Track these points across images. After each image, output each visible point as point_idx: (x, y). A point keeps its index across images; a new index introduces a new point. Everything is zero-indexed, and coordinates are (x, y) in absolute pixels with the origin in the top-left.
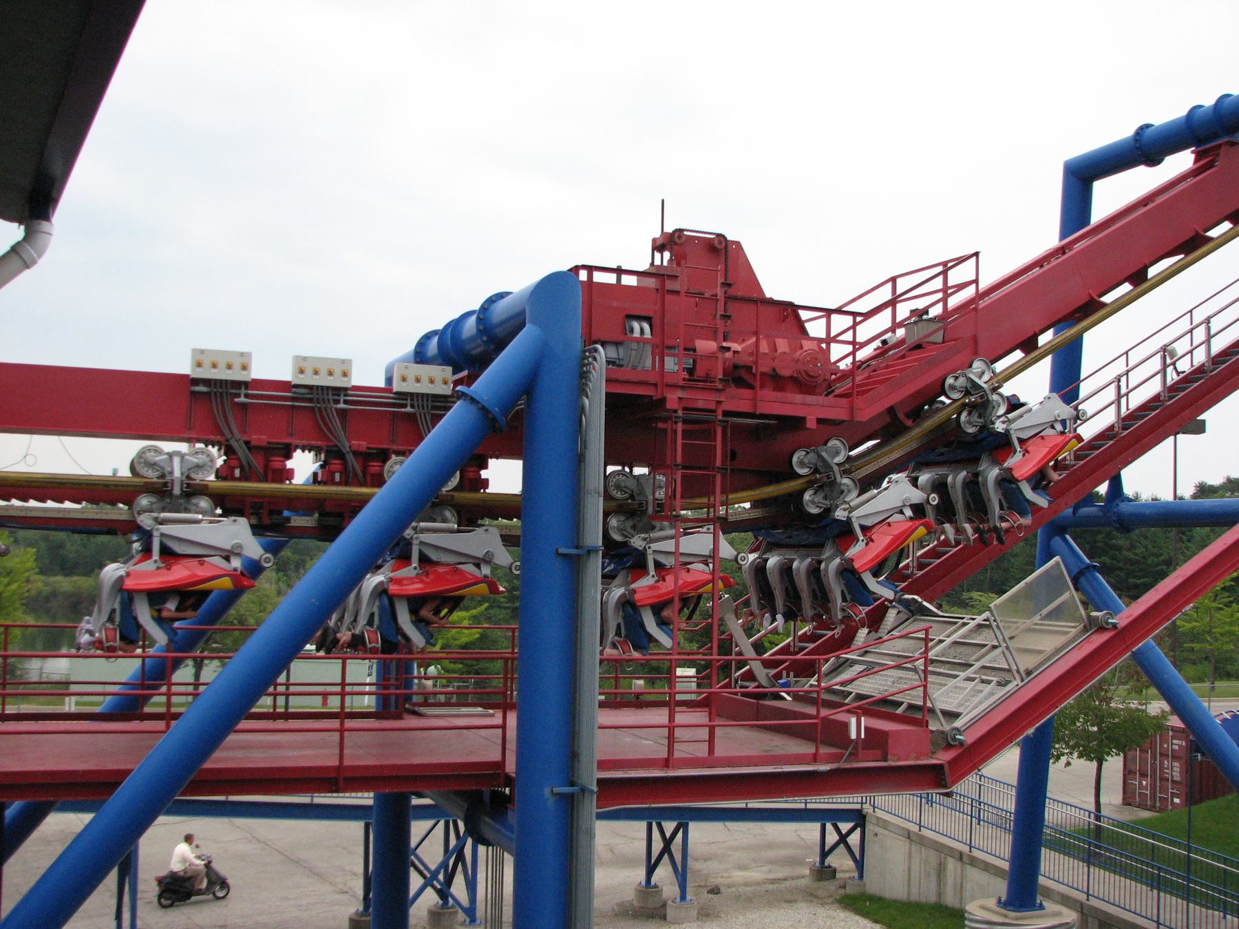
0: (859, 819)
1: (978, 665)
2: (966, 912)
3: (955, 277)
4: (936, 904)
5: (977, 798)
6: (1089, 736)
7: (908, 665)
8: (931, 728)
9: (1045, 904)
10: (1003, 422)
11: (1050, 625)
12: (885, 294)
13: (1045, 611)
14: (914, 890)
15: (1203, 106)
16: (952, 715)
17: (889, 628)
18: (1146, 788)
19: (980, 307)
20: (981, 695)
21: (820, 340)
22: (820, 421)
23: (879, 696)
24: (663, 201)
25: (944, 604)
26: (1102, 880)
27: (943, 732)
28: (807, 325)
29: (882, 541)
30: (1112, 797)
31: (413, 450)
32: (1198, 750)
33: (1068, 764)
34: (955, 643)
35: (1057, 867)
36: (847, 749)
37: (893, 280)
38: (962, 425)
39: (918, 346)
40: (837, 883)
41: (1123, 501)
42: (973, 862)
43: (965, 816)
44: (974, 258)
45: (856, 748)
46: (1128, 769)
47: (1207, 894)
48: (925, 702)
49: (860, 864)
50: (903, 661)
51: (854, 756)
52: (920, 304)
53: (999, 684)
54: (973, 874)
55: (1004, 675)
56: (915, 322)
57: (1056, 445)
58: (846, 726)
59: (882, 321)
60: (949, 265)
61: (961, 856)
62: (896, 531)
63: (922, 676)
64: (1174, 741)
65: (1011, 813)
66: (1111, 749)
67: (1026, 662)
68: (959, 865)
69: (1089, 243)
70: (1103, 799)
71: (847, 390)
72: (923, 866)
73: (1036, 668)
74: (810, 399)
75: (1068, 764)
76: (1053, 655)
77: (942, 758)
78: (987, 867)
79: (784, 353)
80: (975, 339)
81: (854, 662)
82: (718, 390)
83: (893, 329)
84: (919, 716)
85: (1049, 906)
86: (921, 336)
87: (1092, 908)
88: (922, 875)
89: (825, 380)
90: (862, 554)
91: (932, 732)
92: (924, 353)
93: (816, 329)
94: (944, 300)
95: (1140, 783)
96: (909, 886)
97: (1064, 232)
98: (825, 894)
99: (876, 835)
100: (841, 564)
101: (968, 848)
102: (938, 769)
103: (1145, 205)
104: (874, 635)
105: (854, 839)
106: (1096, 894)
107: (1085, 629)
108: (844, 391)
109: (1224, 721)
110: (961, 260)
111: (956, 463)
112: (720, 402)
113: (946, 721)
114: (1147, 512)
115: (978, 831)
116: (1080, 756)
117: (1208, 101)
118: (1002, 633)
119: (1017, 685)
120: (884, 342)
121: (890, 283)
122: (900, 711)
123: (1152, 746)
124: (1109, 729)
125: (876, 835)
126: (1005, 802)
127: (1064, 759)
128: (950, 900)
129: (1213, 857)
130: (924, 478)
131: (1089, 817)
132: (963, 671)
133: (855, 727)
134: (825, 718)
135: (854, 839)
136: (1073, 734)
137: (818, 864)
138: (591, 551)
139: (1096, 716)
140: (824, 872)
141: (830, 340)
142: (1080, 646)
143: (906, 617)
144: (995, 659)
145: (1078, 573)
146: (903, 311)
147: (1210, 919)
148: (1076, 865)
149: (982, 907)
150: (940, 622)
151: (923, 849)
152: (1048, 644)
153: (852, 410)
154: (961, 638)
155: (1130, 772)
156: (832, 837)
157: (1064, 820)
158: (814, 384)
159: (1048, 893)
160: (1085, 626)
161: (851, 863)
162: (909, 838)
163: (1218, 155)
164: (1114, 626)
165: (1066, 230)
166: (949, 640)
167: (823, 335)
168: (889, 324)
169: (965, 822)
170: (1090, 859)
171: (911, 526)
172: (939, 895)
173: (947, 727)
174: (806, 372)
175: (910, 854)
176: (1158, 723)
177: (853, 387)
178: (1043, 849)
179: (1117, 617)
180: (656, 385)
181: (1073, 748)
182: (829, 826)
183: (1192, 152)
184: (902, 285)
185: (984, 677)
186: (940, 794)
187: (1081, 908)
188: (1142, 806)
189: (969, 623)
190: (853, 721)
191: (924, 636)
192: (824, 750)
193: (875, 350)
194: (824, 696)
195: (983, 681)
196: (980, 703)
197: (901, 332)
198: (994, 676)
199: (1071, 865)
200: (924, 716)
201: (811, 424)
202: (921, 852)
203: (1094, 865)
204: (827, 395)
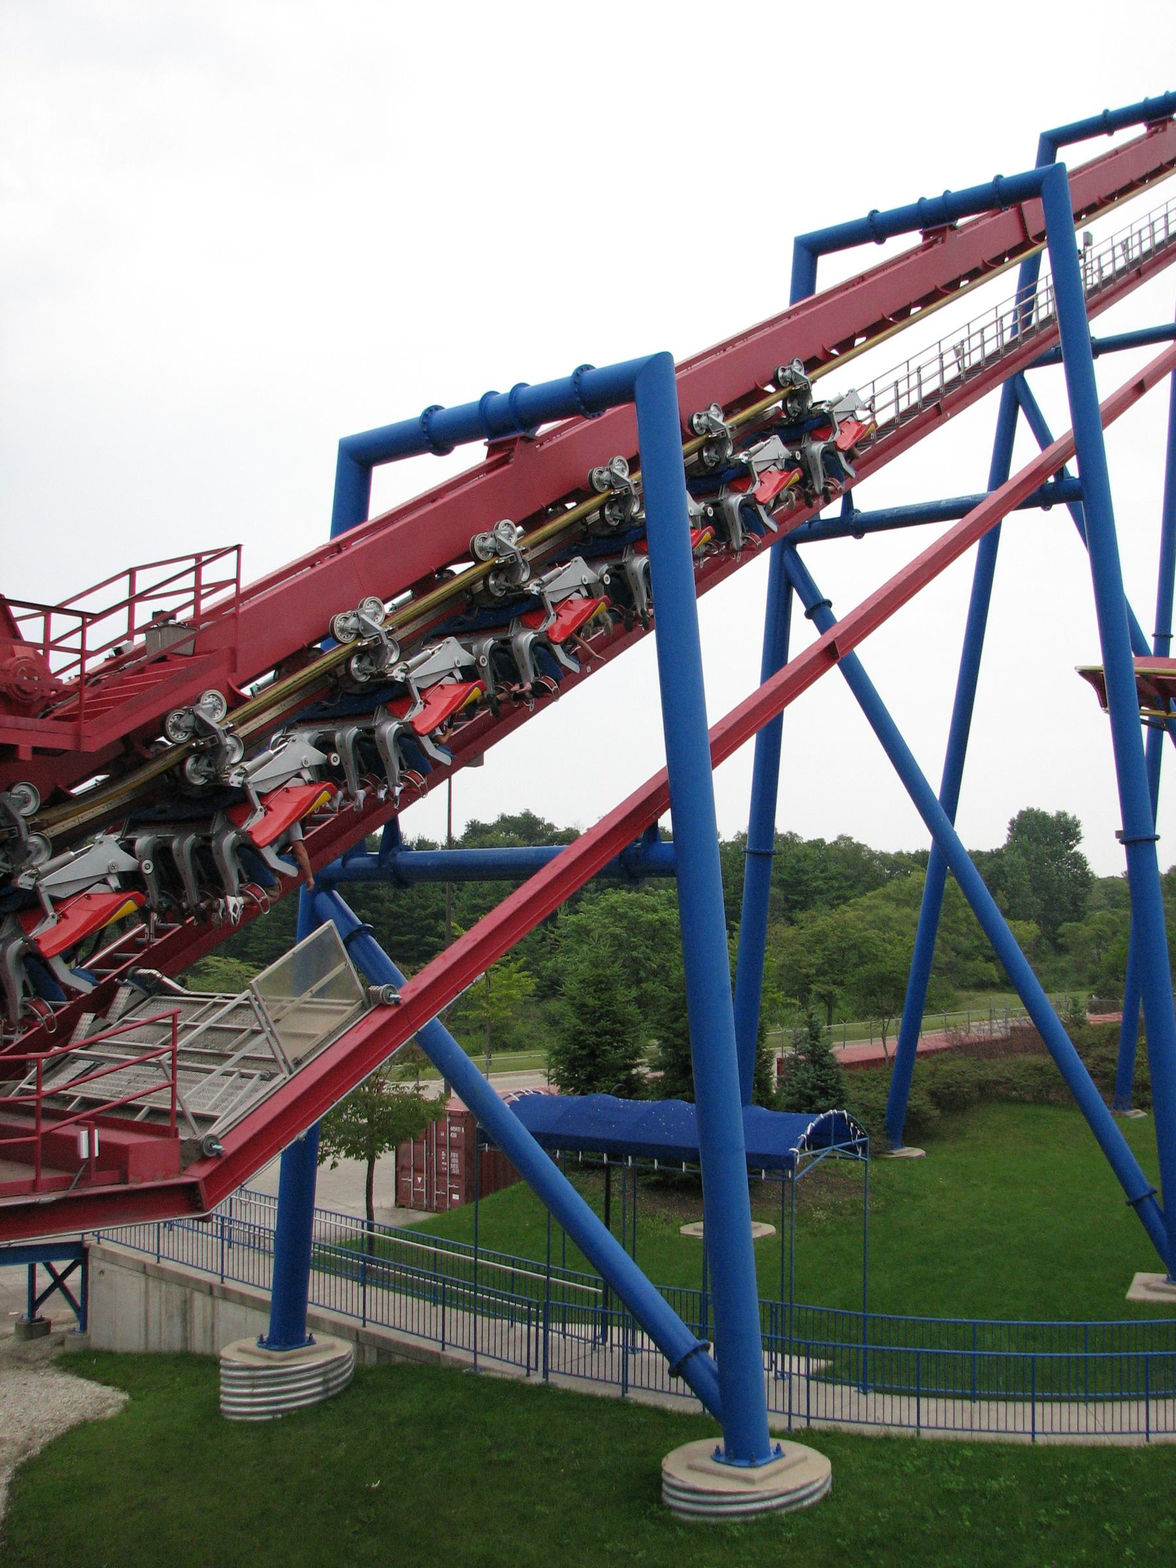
0: (80, 1254)
1: (238, 1055)
2: (221, 1358)
3: (210, 574)
4: (181, 1351)
5: (228, 1216)
6: (360, 1130)
7: (153, 1060)
8: (182, 1137)
9: (315, 1337)
10: (239, 775)
11: (322, 1003)
12: (120, 591)
13: (316, 987)
14: (153, 1337)
15: (497, 393)
16: (205, 1120)
17: (120, 1011)
18: (421, 1185)
19: (241, 610)
20: (242, 1093)
21: (35, 646)
22: (36, 751)
23: (117, 1100)
25: (188, 978)
26: (380, 1301)
27: (196, 1142)
28: (19, 624)
29: (79, 918)
30: (384, 1199)
31: (330, 1322)
32: (485, 1139)
33: (334, 1165)
34: (211, 1029)
35: (327, 1291)
36: (76, 1171)
37: (131, 572)
38: (188, 775)
39: (162, 659)
40: (52, 1339)
41: (401, 850)
42: (226, 1294)
43: (215, 1239)
44: (235, 552)
45: (88, 1169)
46: (400, 1164)
47: (464, 1294)
48: (173, 1105)
49: (82, 1312)
51: (85, 1180)
52: (167, 605)
53: (263, 1078)
54: (228, 1310)
55: (268, 1066)
56: (159, 628)
57: (304, 799)
58: (74, 1142)
59: (115, 626)
60: (204, 558)
61: (210, 1290)
62: (96, 905)
63: (170, 1072)
64: (452, 1128)
65: (270, 1231)
66: (383, 1143)
67: (295, 1049)
68: (208, 1300)
69: (366, 542)
70: (376, 1203)
71: (70, 710)
72: (163, 1308)
73: (307, 1056)
74: (24, 722)
75: (334, 1165)
76: (326, 1040)
77: (197, 1174)
78: (243, 1300)
80: (233, 652)
81: (78, 1057)
83: (130, 635)
84: (165, 1123)
85: (321, 1339)
86: (166, 646)
87: (368, 1334)
88: (163, 1317)
89: (43, 697)
90: (51, 934)
91: (183, 1142)
92: (169, 667)
93: (31, 630)
94: (196, 602)
95: (415, 1180)
96: (147, 1335)
97: (337, 529)
98: (38, 1355)
99: (102, 1272)
100: (22, 947)
101: (220, 1278)
102: (192, 1187)
103: (434, 501)
104: (101, 1022)
105: (74, 1280)
106: (374, 1319)
107: (363, 1007)
108: (65, 712)
109: (513, 1104)
110: (220, 553)
111: (181, 824)
113: (200, 1127)
115: (231, 1257)
116: (348, 1155)
118: (264, 1014)
119: (285, 1079)
120: (118, 651)
121: (128, 577)
122: (139, 1118)
123: (428, 1137)
124: (380, 1119)
125: (102, 1272)
126: (253, 1215)
127: (329, 1160)
128: (199, 1345)
129: (501, 1260)
130: (142, 841)
131: (363, 1228)
132: (220, 1065)
133: (86, 1143)
134: (48, 1135)
135: (74, 1280)
136: (339, 1129)
137: (26, 1317)
139: (366, 1105)
140: (35, 1327)
141: (49, 645)
142: (358, 1027)
143: (142, 997)
144: (257, 1047)
146: (144, 613)
147: (499, 1330)
148: (349, 1286)
149: (241, 1350)
151: (164, 1286)
152: (321, 1026)
153: (78, 737)
154: (217, 1022)
155: (403, 1168)
156: (44, 1280)
157: (328, 1232)
159: (318, 1323)
160: (363, 1003)
161: (69, 1312)
162: (144, 1272)
163: (513, 450)
164: (397, 1002)
165: (338, 526)
166: (203, 1026)
167: (40, 640)
168: (124, 630)
169: (215, 1247)
170: (364, 1277)
171: (118, 900)
172: (186, 1339)
173: (201, 1135)
174: (18, 687)
175: (147, 1292)
176: (437, 1110)
177: (78, 708)
178: (311, 1271)
179: (400, 991)
181: (340, 1145)
182: (40, 1267)
183: (485, 444)
184: (144, 581)
185: (244, 1071)
186: (194, 1219)
187: (356, 1336)
188: (418, 1207)
189: (227, 1003)
190: (84, 1135)
191: (171, 1021)
192: (47, 1175)
193: (106, 660)
194: (45, 1104)
195: (243, 1076)
196: (241, 1102)
197: (140, 639)
198: (255, 1069)
199: (344, 1286)
200: (173, 1123)
201: (25, 755)
202: (160, 1291)
203: (371, 1284)
204: (43, 717)
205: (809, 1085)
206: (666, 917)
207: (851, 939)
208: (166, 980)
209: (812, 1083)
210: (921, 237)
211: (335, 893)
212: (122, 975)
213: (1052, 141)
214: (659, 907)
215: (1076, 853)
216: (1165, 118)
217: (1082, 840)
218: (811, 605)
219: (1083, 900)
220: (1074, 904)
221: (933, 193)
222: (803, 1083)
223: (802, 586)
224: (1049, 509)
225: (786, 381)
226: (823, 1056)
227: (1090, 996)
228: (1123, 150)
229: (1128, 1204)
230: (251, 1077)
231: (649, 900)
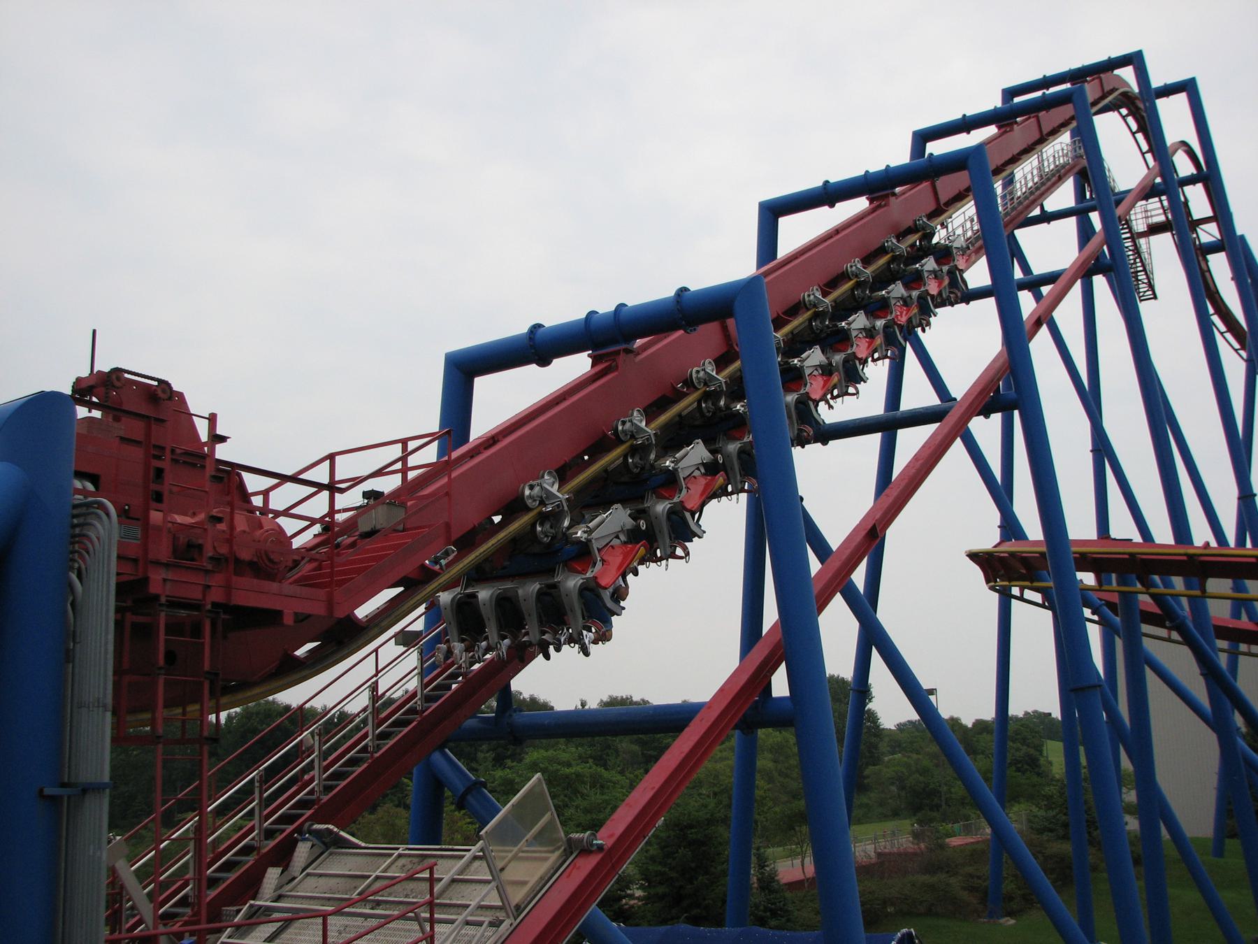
15: (597, 313)
24: (94, 331)
37: (331, 457)
50: (344, 903)
53: (492, 924)
60: (412, 445)
79: (244, 532)
82: (207, 571)
107: (567, 853)
112: (209, 587)
114: (546, 722)
117: (605, 307)
138: (87, 790)
142: (568, 870)
145: (465, 791)
150: (358, 854)
158: (276, 571)
180: (135, 561)
183: (589, 356)
184: (346, 467)
191: (428, 876)
198: (485, 916)
201: (288, 620)
205: (762, 908)
206: (580, 770)
207: (722, 785)
208: (342, 833)
209: (764, 906)
210: (868, 202)
211: (447, 750)
212: (299, 830)
213: (922, 138)
214: (573, 763)
215: (869, 710)
216: (1012, 121)
217: (873, 699)
219: (876, 747)
221: (876, 166)
222: (757, 906)
224: (826, 444)
225: (811, 304)
226: (771, 882)
227: (913, 825)
228: (989, 143)
230: (480, 924)
231: (565, 756)
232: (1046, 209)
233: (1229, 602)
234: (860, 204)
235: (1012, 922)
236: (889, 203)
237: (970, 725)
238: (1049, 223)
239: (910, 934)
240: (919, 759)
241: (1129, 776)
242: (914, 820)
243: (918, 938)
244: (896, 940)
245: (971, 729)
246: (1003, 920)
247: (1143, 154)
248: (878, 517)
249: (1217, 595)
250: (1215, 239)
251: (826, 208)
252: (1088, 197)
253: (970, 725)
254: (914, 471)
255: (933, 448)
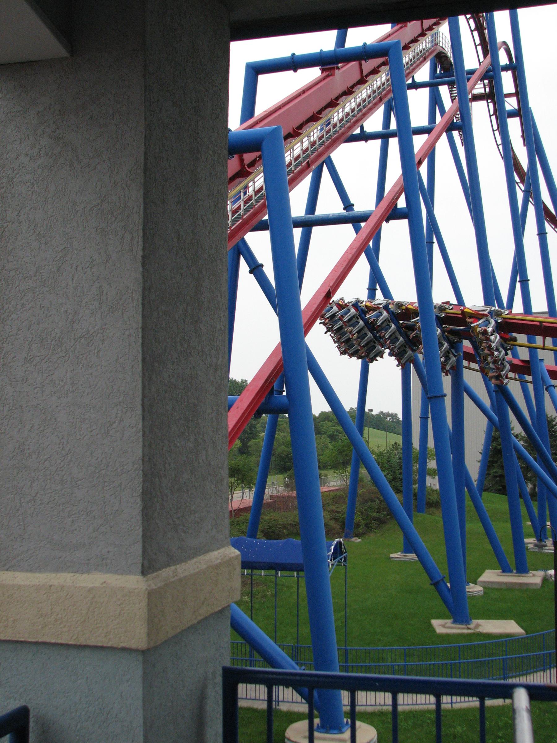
210: (320, 72)
218: (253, 267)
219: (255, 427)
220: (250, 430)
223: (247, 255)
229: (431, 584)
232: (415, 80)
233: (553, 352)
234: (315, 73)
235: (359, 540)
236: (334, 74)
237: (317, 415)
238: (416, 90)
239: (340, 542)
240: (285, 436)
241: (431, 451)
242: (286, 475)
243: (344, 545)
244: (334, 545)
245: (318, 418)
246: (353, 539)
247: (476, 46)
248: (331, 284)
249: (522, 345)
250: (513, 108)
251: (291, 72)
252: (438, 72)
253: (317, 415)
254: (351, 256)
255: (361, 242)
